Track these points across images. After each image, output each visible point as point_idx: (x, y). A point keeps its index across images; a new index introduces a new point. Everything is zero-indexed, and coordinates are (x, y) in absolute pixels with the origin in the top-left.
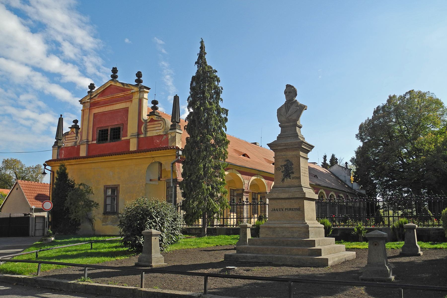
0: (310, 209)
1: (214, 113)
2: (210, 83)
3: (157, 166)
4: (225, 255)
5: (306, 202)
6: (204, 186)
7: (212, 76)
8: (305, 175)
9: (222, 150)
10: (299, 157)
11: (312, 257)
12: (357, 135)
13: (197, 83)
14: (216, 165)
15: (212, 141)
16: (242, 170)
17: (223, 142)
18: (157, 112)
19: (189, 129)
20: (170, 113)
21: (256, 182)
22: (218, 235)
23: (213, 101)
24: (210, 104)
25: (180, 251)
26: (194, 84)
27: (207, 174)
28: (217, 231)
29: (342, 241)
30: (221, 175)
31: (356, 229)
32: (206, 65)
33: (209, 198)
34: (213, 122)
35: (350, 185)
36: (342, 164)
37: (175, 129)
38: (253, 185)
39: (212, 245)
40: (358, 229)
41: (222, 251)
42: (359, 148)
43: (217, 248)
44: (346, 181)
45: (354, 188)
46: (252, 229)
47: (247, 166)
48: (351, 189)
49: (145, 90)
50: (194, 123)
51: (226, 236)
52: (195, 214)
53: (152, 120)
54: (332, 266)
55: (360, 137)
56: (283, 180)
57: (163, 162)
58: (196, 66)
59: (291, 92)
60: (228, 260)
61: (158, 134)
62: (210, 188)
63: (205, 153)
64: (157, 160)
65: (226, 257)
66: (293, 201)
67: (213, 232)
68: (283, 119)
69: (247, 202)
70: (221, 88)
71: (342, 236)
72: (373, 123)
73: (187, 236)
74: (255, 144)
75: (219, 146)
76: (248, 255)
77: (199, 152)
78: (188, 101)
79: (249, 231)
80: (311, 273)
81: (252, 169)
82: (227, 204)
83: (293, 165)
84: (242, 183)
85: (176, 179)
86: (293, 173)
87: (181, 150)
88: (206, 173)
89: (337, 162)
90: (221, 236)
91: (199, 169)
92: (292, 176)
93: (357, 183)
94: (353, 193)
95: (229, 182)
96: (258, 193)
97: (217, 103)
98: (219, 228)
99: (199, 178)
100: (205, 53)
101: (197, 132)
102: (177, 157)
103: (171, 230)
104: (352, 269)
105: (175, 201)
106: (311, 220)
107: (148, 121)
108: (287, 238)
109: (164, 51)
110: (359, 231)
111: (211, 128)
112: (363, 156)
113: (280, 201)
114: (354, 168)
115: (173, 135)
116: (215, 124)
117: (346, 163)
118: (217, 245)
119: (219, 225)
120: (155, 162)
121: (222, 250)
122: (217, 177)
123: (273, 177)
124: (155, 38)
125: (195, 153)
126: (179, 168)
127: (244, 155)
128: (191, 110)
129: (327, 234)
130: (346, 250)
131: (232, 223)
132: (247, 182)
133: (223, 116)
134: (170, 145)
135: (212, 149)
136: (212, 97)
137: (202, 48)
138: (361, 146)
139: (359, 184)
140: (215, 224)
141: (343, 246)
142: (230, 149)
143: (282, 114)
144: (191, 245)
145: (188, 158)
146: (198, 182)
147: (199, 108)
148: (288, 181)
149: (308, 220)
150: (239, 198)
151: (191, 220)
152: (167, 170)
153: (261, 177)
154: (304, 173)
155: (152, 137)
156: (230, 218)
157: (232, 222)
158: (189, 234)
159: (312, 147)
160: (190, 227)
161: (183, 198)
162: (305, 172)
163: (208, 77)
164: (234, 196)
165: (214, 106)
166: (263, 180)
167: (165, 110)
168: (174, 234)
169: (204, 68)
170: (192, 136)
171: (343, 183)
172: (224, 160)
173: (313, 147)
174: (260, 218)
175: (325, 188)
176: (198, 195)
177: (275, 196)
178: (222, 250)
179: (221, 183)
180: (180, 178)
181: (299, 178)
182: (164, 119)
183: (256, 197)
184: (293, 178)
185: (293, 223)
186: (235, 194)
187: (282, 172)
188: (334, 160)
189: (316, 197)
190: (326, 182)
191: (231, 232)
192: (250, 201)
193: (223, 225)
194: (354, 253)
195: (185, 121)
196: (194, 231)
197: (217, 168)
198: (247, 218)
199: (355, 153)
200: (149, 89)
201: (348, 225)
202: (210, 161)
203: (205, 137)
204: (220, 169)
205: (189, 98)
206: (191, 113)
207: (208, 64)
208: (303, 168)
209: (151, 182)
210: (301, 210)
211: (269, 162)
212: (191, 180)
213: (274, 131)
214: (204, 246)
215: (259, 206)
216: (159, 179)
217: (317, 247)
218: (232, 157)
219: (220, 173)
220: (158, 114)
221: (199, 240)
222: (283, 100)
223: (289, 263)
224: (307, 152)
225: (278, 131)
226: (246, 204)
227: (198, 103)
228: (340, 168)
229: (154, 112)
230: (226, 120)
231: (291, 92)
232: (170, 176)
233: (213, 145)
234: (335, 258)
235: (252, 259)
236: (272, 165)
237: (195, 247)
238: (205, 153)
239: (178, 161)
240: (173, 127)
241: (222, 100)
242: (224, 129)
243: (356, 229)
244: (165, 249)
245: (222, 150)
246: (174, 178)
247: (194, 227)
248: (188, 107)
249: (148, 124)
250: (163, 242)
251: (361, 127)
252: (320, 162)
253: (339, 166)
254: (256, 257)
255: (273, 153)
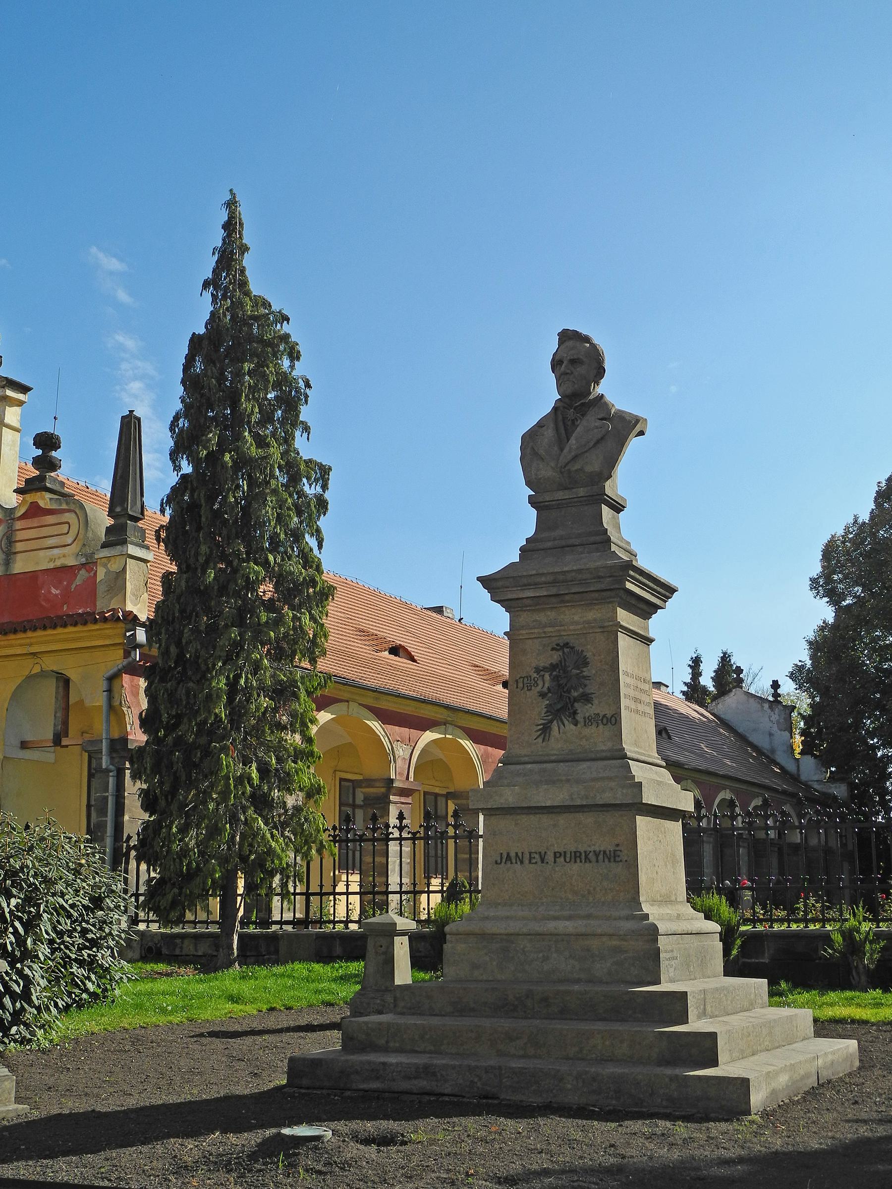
0: (660, 853)
1: (272, 476)
2: (262, 364)
3: (50, 689)
4: (292, 1060)
5: (641, 821)
6: (230, 764)
7: (268, 337)
8: (641, 707)
9: (306, 620)
10: (612, 630)
11: (677, 1071)
12: (814, 583)
13: (209, 361)
14: (280, 682)
15: (267, 590)
16: (386, 704)
17: (308, 591)
18: (55, 480)
19: (175, 539)
20: (105, 487)
21: (439, 754)
22: (284, 963)
23: (274, 434)
24: (261, 442)
25: (109, 1036)
26: (199, 366)
27: (241, 716)
28: (283, 947)
29: (783, 985)
30: (301, 723)
31: (838, 938)
32: (247, 293)
33: (250, 812)
34: (269, 511)
35: (791, 767)
36: (760, 686)
37: (124, 542)
38: (428, 763)
39: (251, 1009)
40: (848, 935)
41: (286, 1037)
42: (822, 629)
43: (271, 1022)
44: (773, 751)
45: (803, 778)
46: (414, 938)
47: (405, 691)
48: (794, 778)
49: (9, 393)
50: (195, 520)
51: (317, 967)
52: (191, 876)
53: (35, 511)
54: (765, 1114)
55: (824, 585)
56: (545, 730)
57: (72, 674)
58: (208, 296)
59: (578, 361)
60: (305, 1082)
61: (58, 563)
62: (255, 775)
63: (234, 633)
64: (51, 664)
65: (298, 1068)
66: (588, 819)
67: (263, 950)
68: (547, 472)
69: (401, 829)
70: (301, 384)
71: (790, 967)
72: (874, 535)
73: (161, 967)
74: (439, 610)
75: (292, 608)
76: (393, 1059)
77: (213, 629)
78: (172, 429)
79: (402, 948)
80: (676, 1155)
81: (424, 701)
82: (324, 837)
83: (586, 663)
84: (385, 757)
85: (124, 740)
86: (586, 698)
87: (143, 625)
88: (237, 715)
89: (742, 681)
90: (297, 966)
91: (209, 697)
92: (585, 711)
93: (815, 757)
94: (796, 791)
95: (338, 752)
96: (449, 796)
97: (288, 440)
98: (288, 935)
99: (213, 731)
100: (244, 249)
101: (204, 549)
102: (127, 654)
103: (80, 949)
104: (863, 1131)
105: (119, 827)
106: (666, 900)
107: (19, 513)
108: (561, 981)
109: (122, 296)
110: (853, 945)
111: (262, 536)
112: (838, 658)
113: (533, 819)
114: (803, 702)
115: (115, 566)
116: (279, 519)
117: (775, 685)
118: (272, 1009)
119: (294, 923)
120: (43, 674)
121: (288, 1030)
122: (284, 728)
123: (504, 731)
124: (94, 250)
125: (196, 631)
126: (136, 695)
127: (395, 650)
128: (187, 468)
129: (734, 968)
130: (818, 1034)
131: (341, 914)
132: (405, 752)
133: (310, 490)
134: (103, 604)
135: (264, 619)
136: (267, 418)
137: (231, 226)
138: (831, 620)
139: (825, 761)
140: (276, 917)
141: (799, 1013)
142: (334, 615)
143: (542, 452)
144: (163, 1011)
145: (165, 653)
146: (207, 752)
147: (214, 458)
148: (565, 736)
149: (653, 902)
150: (370, 812)
151: (174, 904)
152: (88, 703)
153: (459, 732)
154: (637, 700)
155: (33, 576)
156: (334, 894)
157: (345, 907)
158: (171, 959)
159: (667, 591)
160: (176, 930)
161: (146, 816)
162: (638, 695)
163: (250, 338)
164: (354, 806)
165: (275, 451)
166: (467, 744)
167: (87, 473)
168: (90, 964)
169: (237, 305)
170: (185, 566)
171: (766, 758)
172: (313, 661)
173: (672, 590)
174: (452, 895)
175: (704, 777)
176: (205, 803)
177: (509, 796)
178: (288, 1030)
179: (298, 755)
180: (138, 737)
181: (614, 720)
182: (82, 507)
183: (441, 812)
184: (589, 721)
185: (589, 917)
186: (359, 800)
187: (543, 695)
188: (728, 675)
189: (686, 801)
190: (702, 755)
191: (338, 950)
192: (413, 822)
193: (305, 922)
194: (852, 1045)
195: (163, 511)
196: (188, 948)
197: (283, 692)
198: (401, 893)
199: (806, 646)
200: (24, 389)
201: (806, 921)
202: (257, 667)
203: (235, 571)
204: (296, 696)
205: (176, 418)
206: (184, 477)
207: (256, 288)
208: (628, 680)
209: (28, 754)
210: (623, 858)
211: (491, 676)
212: (179, 742)
213: (508, 526)
214: (216, 1012)
215: (451, 843)
216: (57, 741)
217: (696, 1024)
218: (344, 648)
219: (293, 715)
220: (56, 487)
221: (201, 987)
222: (546, 395)
223: (573, 1099)
224: (647, 610)
225: (527, 522)
226: (396, 834)
227: (213, 437)
228: (754, 704)
229: (41, 479)
230: (322, 505)
231: (578, 361)
232: (101, 729)
233: (270, 606)
234: (777, 1073)
235: (408, 1078)
236: (500, 687)
237: (176, 1019)
238: (234, 633)
239: (133, 670)
240: (117, 536)
241: (306, 429)
242: (312, 542)
243: (838, 938)
244: (40, 1033)
245: (306, 620)
246: (116, 735)
247: (189, 929)
248: (174, 456)
249: (18, 525)
250: (30, 1002)
251: (829, 552)
252: (678, 680)
253: (748, 694)
254: (427, 1071)
255: (498, 620)
